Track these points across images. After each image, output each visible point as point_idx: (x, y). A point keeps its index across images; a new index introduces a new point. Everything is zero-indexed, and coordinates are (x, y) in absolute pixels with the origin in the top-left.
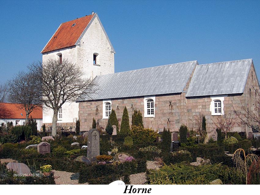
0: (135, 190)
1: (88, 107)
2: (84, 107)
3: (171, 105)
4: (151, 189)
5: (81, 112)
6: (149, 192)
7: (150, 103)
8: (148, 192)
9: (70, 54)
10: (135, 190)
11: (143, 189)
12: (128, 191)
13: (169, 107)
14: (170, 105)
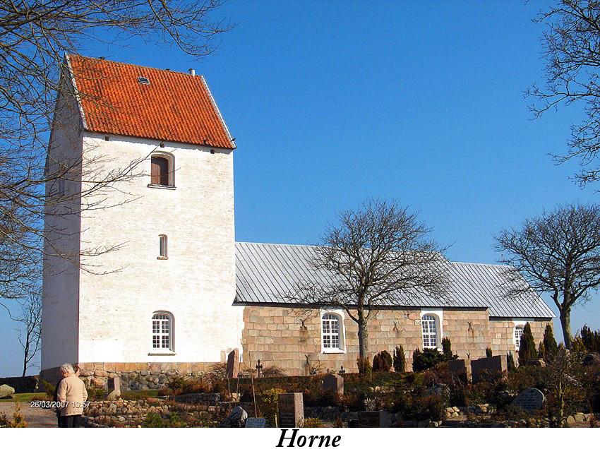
0: (303, 439)
1: (277, 321)
2: (262, 319)
4: (340, 437)
5: (251, 333)
6: (336, 444)
7: (330, 323)
8: (334, 445)
9: (209, 167)
10: (301, 444)
11: (323, 437)
12: (286, 442)
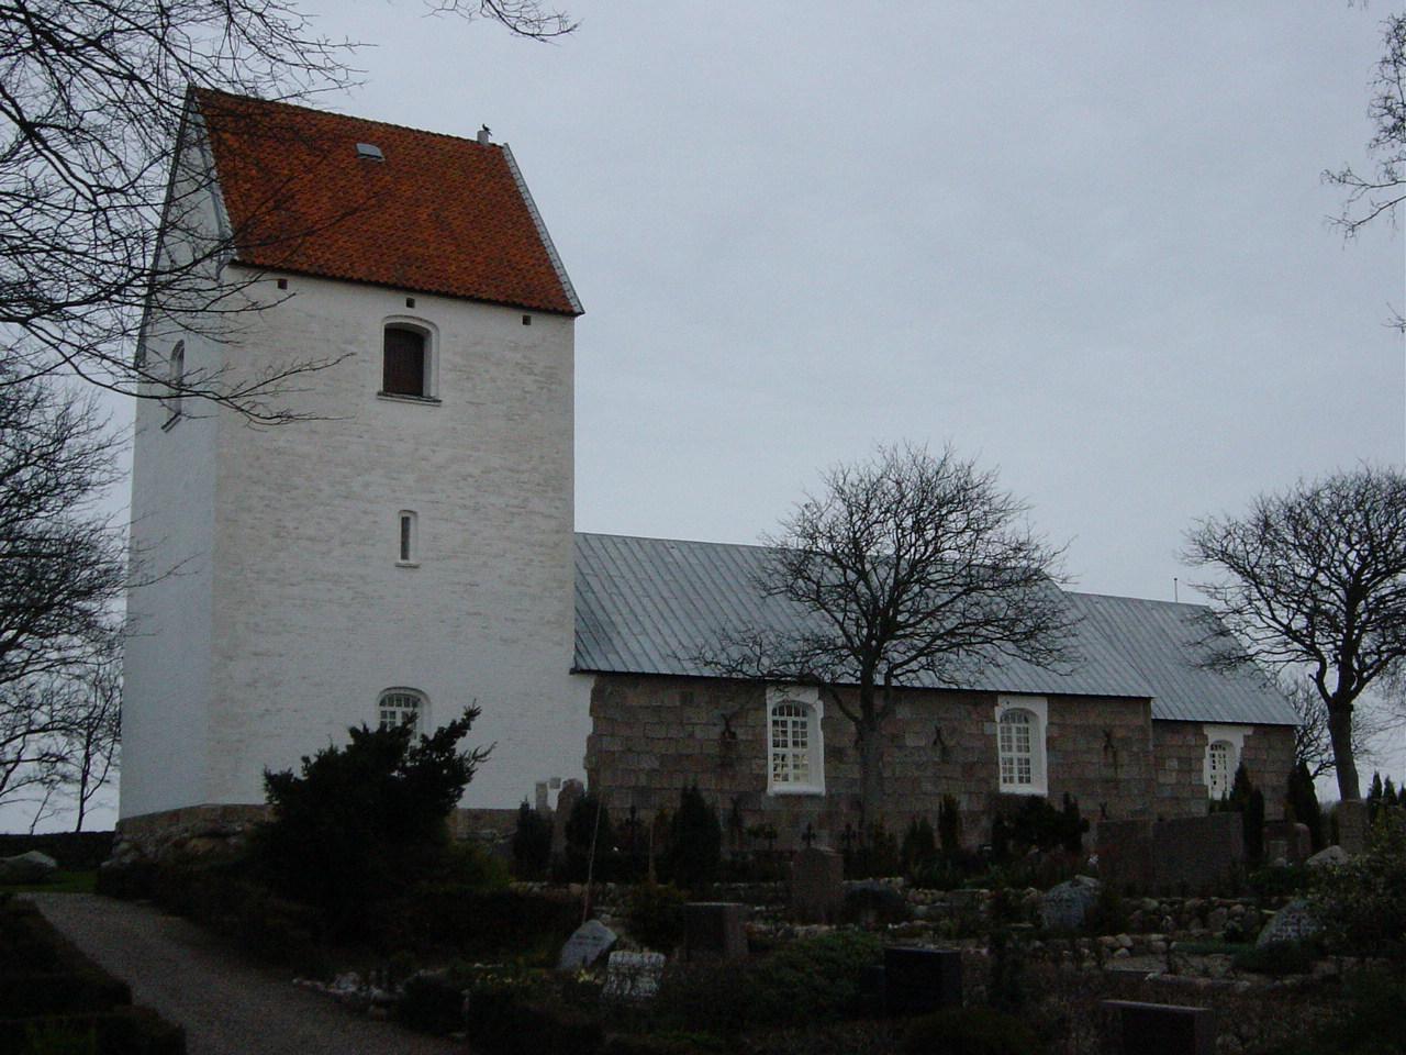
3: (1112, 747)
5: (606, 744)
7: (790, 724)
13: (1103, 753)
14: (1106, 748)
